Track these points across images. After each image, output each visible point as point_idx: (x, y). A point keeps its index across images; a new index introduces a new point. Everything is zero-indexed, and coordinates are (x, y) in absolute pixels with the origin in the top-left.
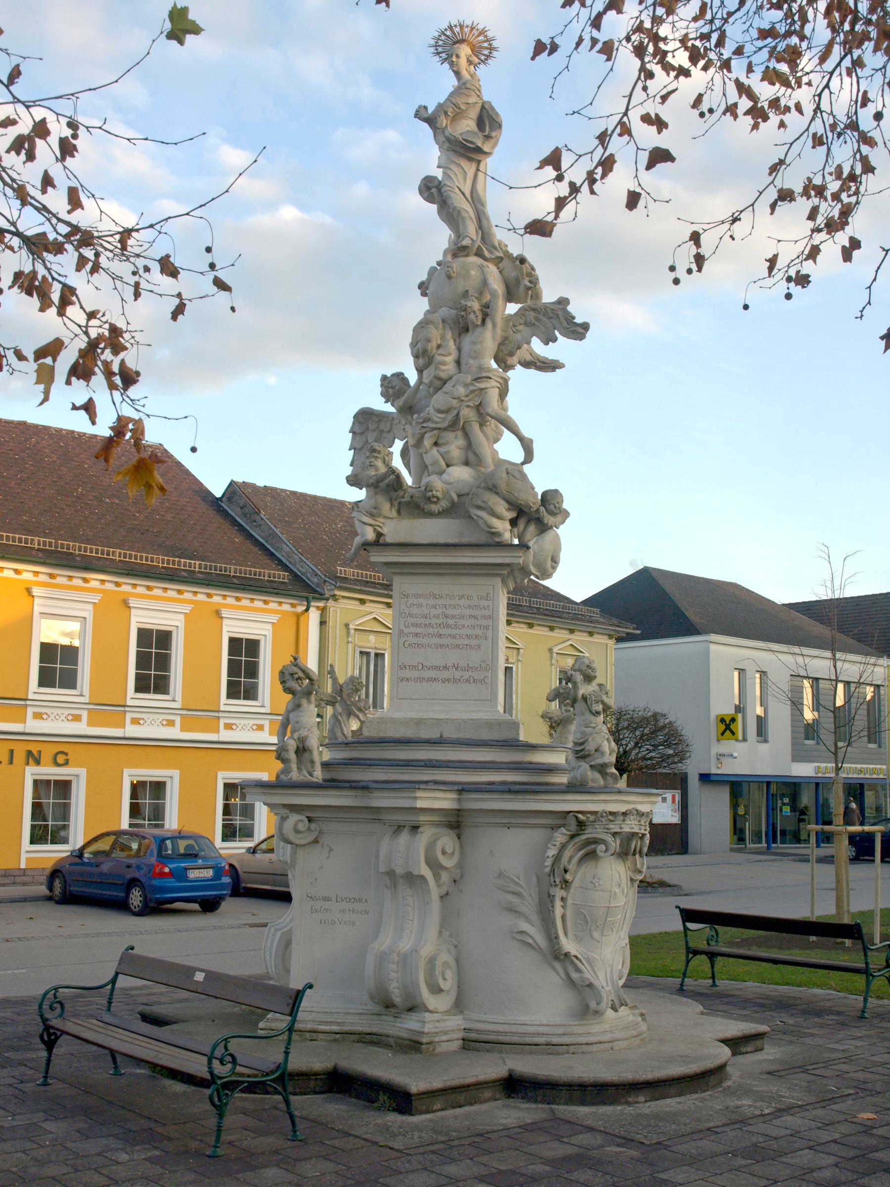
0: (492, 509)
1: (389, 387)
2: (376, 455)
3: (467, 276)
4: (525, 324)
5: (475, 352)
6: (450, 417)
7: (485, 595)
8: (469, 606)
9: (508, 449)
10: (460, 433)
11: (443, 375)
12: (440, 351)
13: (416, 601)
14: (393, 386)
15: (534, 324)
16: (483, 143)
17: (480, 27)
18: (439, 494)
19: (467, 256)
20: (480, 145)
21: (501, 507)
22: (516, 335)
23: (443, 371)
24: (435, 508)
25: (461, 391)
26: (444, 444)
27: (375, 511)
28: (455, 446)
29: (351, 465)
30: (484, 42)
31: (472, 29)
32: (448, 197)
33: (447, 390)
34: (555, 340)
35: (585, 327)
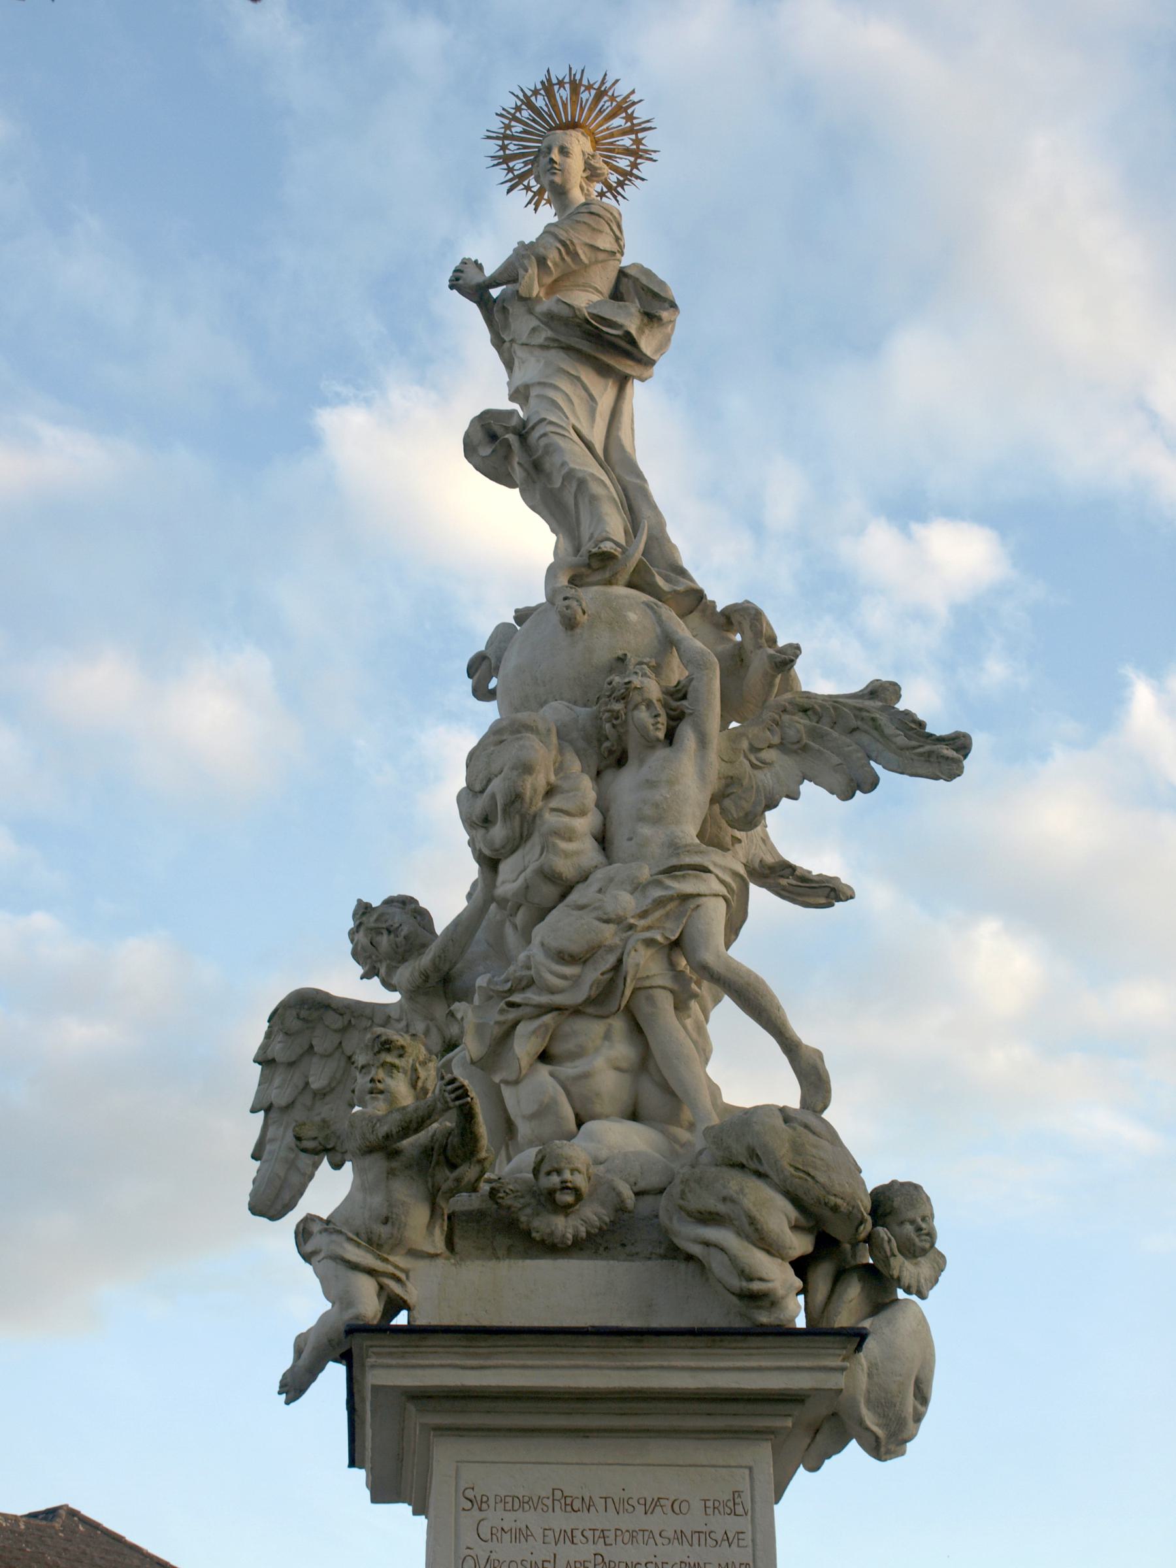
0: (752, 1221)
1: (378, 931)
2: (390, 1058)
3: (617, 622)
4: (782, 747)
5: (657, 805)
6: (594, 975)
7: (727, 1496)
8: (680, 1536)
9: (743, 1073)
10: (618, 1025)
11: (565, 868)
12: (555, 803)
13: (509, 1520)
14: (387, 933)
15: (805, 748)
16: (641, 330)
17: (621, 90)
18: (580, 1181)
19: (609, 582)
20: (633, 332)
21: (778, 1216)
22: (759, 774)
23: (567, 855)
24: (564, 1227)
25: (626, 902)
26: (573, 1056)
27: (383, 1231)
28: (605, 1057)
29: (255, 1156)
30: (625, 132)
31: (601, 94)
32: (549, 450)
33: (583, 901)
34: (870, 784)
35: (961, 744)
